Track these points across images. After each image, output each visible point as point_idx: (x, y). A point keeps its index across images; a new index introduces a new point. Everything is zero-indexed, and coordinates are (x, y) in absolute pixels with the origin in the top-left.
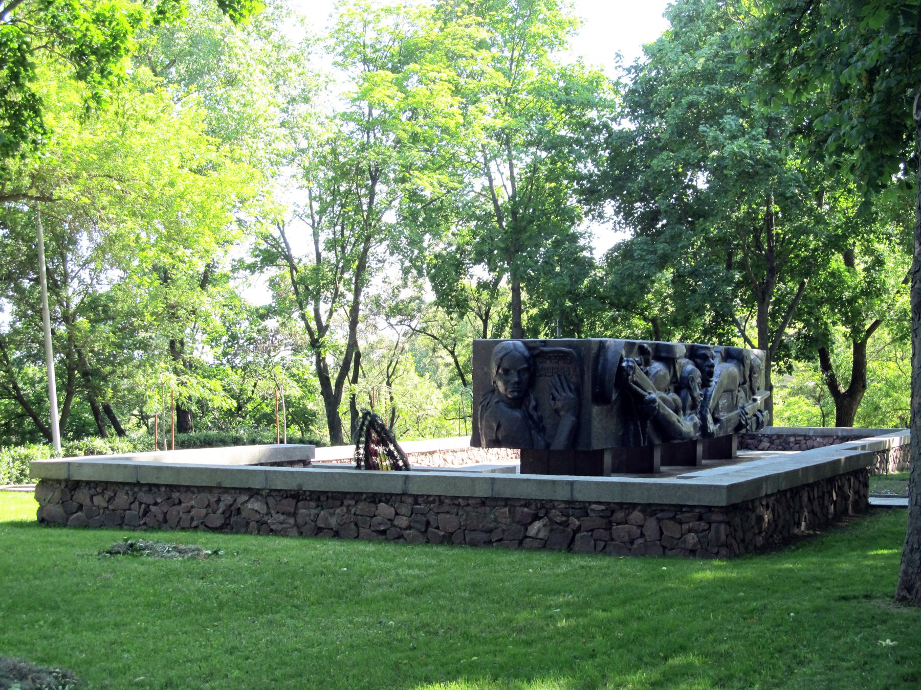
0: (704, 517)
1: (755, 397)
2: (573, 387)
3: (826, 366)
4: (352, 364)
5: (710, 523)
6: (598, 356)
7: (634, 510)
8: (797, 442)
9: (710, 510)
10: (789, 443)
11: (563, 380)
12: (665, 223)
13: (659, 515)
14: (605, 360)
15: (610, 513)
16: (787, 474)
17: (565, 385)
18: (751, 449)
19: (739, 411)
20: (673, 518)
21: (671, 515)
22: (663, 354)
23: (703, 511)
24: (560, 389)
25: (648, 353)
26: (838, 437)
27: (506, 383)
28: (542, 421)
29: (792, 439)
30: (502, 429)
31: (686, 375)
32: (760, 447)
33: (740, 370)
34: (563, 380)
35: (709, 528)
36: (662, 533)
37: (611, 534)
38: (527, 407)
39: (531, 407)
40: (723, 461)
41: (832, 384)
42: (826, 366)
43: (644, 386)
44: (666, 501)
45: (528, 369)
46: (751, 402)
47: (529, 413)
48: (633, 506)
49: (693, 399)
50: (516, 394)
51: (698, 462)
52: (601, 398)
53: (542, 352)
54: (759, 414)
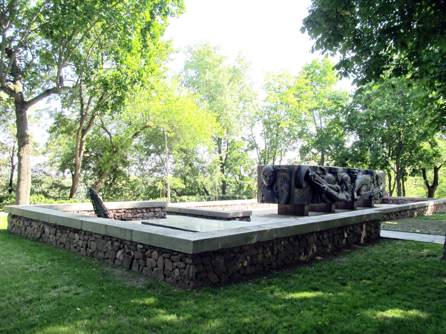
3: (425, 178)
5: (186, 264)
7: (154, 250)
8: (402, 202)
12: (366, 131)
13: (163, 255)
14: (300, 172)
15: (145, 251)
16: (272, 230)
19: (371, 191)
20: (169, 258)
21: (168, 255)
22: (333, 171)
23: (182, 255)
25: (325, 170)
27: (266, 180)
29: (400, 201)
35: (185, 267)
36: (164, 267)
37: (146, 263)
40: (284, 216)
41: (427, 183)
42: (425, 178)
43: (320, 181)
44: (166, 247)
48: (155, 248)
49: (347, 187)
51: (305, 213)
52: (299, 186)
53: (278, 169)
54: (381, 192)
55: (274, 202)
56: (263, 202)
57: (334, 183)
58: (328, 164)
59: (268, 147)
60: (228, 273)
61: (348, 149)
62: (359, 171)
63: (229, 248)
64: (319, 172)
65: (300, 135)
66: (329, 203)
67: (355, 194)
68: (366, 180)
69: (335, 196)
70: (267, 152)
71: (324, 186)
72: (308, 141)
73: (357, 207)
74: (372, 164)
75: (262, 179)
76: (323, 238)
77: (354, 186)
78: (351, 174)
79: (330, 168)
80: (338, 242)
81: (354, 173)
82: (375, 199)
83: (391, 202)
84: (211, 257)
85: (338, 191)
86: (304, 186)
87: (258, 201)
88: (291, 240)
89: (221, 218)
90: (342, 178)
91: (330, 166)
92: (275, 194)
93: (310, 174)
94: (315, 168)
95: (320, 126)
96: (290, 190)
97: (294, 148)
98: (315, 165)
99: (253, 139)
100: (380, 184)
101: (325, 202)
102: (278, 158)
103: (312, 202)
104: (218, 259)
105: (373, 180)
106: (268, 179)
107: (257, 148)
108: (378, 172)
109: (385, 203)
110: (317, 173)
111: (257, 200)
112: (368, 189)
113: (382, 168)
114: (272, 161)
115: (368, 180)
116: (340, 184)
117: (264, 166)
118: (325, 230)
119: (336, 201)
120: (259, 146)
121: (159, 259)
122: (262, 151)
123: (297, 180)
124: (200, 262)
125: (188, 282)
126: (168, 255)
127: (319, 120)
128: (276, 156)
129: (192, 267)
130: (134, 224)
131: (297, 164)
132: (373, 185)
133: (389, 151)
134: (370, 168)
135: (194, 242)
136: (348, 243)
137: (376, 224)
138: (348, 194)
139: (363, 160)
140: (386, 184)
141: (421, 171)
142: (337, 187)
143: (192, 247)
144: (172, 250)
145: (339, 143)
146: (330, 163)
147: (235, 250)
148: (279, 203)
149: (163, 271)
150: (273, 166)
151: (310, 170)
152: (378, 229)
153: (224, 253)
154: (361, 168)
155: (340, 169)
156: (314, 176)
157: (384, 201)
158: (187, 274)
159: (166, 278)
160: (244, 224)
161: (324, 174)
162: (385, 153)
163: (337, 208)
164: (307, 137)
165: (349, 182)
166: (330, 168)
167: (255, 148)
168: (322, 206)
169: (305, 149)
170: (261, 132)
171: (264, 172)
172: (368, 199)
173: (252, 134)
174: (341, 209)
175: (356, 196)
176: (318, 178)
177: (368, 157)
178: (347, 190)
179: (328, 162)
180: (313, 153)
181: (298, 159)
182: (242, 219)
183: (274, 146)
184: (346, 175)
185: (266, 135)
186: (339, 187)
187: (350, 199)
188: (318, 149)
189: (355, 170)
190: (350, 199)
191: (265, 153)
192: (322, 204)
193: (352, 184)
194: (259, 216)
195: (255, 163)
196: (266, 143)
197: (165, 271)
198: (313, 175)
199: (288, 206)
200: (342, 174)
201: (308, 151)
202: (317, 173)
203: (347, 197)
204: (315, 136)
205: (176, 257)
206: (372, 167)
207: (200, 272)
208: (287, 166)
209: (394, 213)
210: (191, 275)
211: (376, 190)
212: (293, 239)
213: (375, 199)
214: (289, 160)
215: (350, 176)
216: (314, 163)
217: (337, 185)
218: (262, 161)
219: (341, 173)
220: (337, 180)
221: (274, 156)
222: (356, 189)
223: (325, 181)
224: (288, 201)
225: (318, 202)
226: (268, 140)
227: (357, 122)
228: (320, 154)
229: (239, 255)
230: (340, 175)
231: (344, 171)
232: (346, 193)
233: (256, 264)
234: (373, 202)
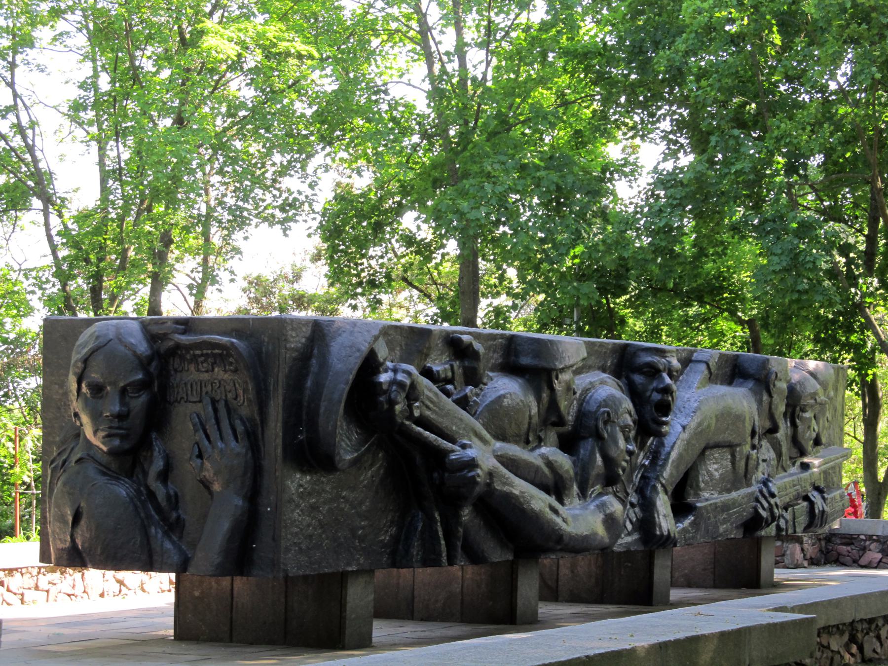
1: (806, 460)
2: (240, 428)
6: (305, 357)
11: (223, 413)
14: (324, 364)
17: (225, 424)
18: (844, 565)
19: (754, 488)
22: (525, 360)
25: (475, 355)
27: (96, 417)
30: (83, 522)
31: (593, 407)
32: (863, 561)
33: (760, 402)
34: (223, 413)
38: (145, 474)
43: (443, 422)
45: (143, 386)
46: (794, 470)
47: (147, 488)
49: (609, 461)
50: (117, 442)
51: (656, 596)
52: (312, 455)
53: (178, 346)
54: (816, 497)
55: (149, 564)
56: (75, 558)
57: (529, 438)
58: (498, 312)
59: (116, 197)
61: (628, 222)
62: (687, 361)
64: (439, 366)
65: (333, 119)
67: (663, 504)
68: (730, 418)
69: (535, 518)
70: (112, 227)
71: (470, 453)
72: (377, 161)
73: (674, 584)
74: (765, 317)
75: (76, 405)
77: (656, 456)
78: (638, 379)
79: (512, 344)
81: (653, 372)
82: (780, 535)
85: (556, 488)
86: (346, 454)
87: (44, 556)
90: (582, 402)
91: (516, 328)
93: (384, 378)
94: (414, 340)
95: (453, 67)
96: (254, 484)
97: (290, 206)
98: (422, 322)
99: (17, 142)
101: (475, 557)
102: (184, 269)
103: (397, 556)
105: (771, 417)
106: (113, 406)
107: (47, 200)
108: (803, 366)
109: (838, 561)
110: (427, 373)
111: (34, 546)
112: (740, 476)
113: (826, 343)
114: (145, 291)
115: (739, 418)
116: (567, 444)
117: (88, 322)
119: (547, 550)
120: (60, 187)
122: (83, 217)
123: (301, 413)
127: (451, 31)
128: (171, 257)
130: (673, 461)
131: (310, 314)
132: (767, 452)
133: (871, 240)
134: (754, 344)
138: (616, 507)
139: (714, 293)
140: (848, 442)
142: (549, 464)
145: (572, 188)
146: (509, 305)
148: (181, 568)
150: (145, 326)
151: (382, 352)
154: (704, 339)
155: (572, 346)
156: (412, 393)
157: (834, 551)
161: (473, 378)
162: (845, 250)
163: (552, 592)
164: (374, 136)
165: (624, 429)
166: (512, 340)
167: (37, 203)
168: (456, 588)
169: (361, 216)
170: (75, 93)
171: (86, 361)
172: (737, 534)
173: (14, 108)
174: (575, 598)
175: (665, 520)
177: (745, 276)
178: (610, 479)
179: (504, 301)
180: (409, 240)
181: (316, 281)
183: (151, 185)
184: (606, 388)
185: (107, 110)
186: (564, 461)
187: (627, 540)
188: (438, 216)
189: (661, 352)
190: (627, 540)
191: (98, 231)
192: (456, 570)
193: (641, 447)
194: (54, 655)
195: (35, 301)
196: (110, 165)
198: (401, 385)
199: (239, 582)
200: (581, 382)
201: (378, 228)
202: (427, 373)
203: (610, 521)
204: (424, 135)
206: (766, 339)
208: (236, 326)
211: (786, 483)
213: (780, 535)
214: (257, 282)
215: (634, 393)
216: (408, 309)
217: (550, 451)
218: (79, 284)
219: (578, 372)
220: (551, 414)
221: (160, 257)
222: (668, 473)
223: (478, 426)
224: (241, 555)
225: (431, 560)
226: (121, 152)
227: (681, 45)
228: (452, 247)
230: (569, 389)
231: (595, 360)
232: (609, 499)
234: (767, 558)
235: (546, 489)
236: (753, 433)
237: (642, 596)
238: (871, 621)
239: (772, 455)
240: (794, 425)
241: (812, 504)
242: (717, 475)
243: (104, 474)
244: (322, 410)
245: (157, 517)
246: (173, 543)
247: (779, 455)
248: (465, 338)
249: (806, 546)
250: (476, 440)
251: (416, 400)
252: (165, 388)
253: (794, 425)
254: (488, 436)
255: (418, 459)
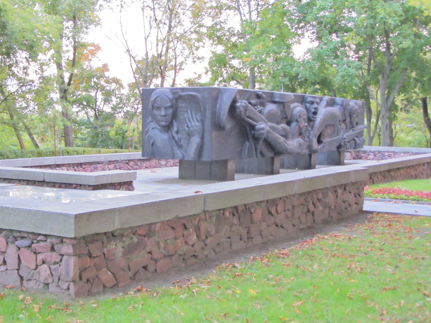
0: (55, 247)
2: (199, 119)
4: (243, 122)
9: (62, 242)
10: (384, 156)
13: (17, 243)
17: (194, 117)
21: (27, 242)
22: (277, 100)
24: (191, 120)
25: (263, 98)
26: (413, 153)
28: (181, 141)
32: (368, 158)
35: (61, 260)
38: (172, 132)
39: (174, 132)
45: (171, 107)
54: (356, 139)
60: (129, 269)
63: (131, 228)
66: (271, 156)
76: (277, 211)
78: (308, 105)
80: (299, 218)
83: (371, 156)
84: (103, 243)
85: (286, 136)
88: (227, 214)
89: (81, 185)
92: (176, 142)
100: (355, 125)
104: (113, 247)
110: (250, 103)
118: (280, 199)
121: (9, 251)
124: (86, 252)
125: (65, 286)
126: (27, 242)
129: (72, 260)
132: (343, 126)
135: (76, 216)
136: (314, 221)
137: (358, 189)
141: (420, 102)
143: (73, 226)
144: (33, 233)
147: (140, 232)
149: (18, 270)
151: (238, 97)
152: (359, 195)
153: (123, 235)
156: (246, 109)
158: (64, 273)
159: (24, 282)
160: (122, 194)
175: (315, 146)
176: (254, 111)
182: (118, 186)
197: (20, 271)
205: (42, 244)
207: (85, 269)
209: (380, 173)
210: (72, 273)
212: (230, 212)
217: (284, 125)
229: (146, 239)
233: (172, 255)
235: (283, 136)
236: (340, 121)
237: (309, 166)
238: (375, 173)
239: (345, 127)
240: (351, 118)
241: (356, 141)
242: (330, 133)
243: (160, 132)
244: (222, 114)
245: (175, 144)
246: (180, 151)
247: (347, 127)
248: (260, 93)
249: (352, 154)
250: (263, 122)
251: (247, 111)
252: (177, 108)
253: (351, 118)
254: (267, 121)
255: (248, 128)
